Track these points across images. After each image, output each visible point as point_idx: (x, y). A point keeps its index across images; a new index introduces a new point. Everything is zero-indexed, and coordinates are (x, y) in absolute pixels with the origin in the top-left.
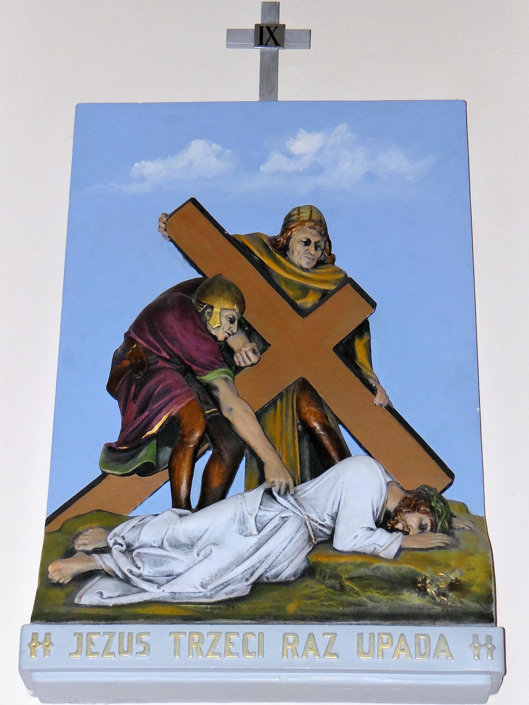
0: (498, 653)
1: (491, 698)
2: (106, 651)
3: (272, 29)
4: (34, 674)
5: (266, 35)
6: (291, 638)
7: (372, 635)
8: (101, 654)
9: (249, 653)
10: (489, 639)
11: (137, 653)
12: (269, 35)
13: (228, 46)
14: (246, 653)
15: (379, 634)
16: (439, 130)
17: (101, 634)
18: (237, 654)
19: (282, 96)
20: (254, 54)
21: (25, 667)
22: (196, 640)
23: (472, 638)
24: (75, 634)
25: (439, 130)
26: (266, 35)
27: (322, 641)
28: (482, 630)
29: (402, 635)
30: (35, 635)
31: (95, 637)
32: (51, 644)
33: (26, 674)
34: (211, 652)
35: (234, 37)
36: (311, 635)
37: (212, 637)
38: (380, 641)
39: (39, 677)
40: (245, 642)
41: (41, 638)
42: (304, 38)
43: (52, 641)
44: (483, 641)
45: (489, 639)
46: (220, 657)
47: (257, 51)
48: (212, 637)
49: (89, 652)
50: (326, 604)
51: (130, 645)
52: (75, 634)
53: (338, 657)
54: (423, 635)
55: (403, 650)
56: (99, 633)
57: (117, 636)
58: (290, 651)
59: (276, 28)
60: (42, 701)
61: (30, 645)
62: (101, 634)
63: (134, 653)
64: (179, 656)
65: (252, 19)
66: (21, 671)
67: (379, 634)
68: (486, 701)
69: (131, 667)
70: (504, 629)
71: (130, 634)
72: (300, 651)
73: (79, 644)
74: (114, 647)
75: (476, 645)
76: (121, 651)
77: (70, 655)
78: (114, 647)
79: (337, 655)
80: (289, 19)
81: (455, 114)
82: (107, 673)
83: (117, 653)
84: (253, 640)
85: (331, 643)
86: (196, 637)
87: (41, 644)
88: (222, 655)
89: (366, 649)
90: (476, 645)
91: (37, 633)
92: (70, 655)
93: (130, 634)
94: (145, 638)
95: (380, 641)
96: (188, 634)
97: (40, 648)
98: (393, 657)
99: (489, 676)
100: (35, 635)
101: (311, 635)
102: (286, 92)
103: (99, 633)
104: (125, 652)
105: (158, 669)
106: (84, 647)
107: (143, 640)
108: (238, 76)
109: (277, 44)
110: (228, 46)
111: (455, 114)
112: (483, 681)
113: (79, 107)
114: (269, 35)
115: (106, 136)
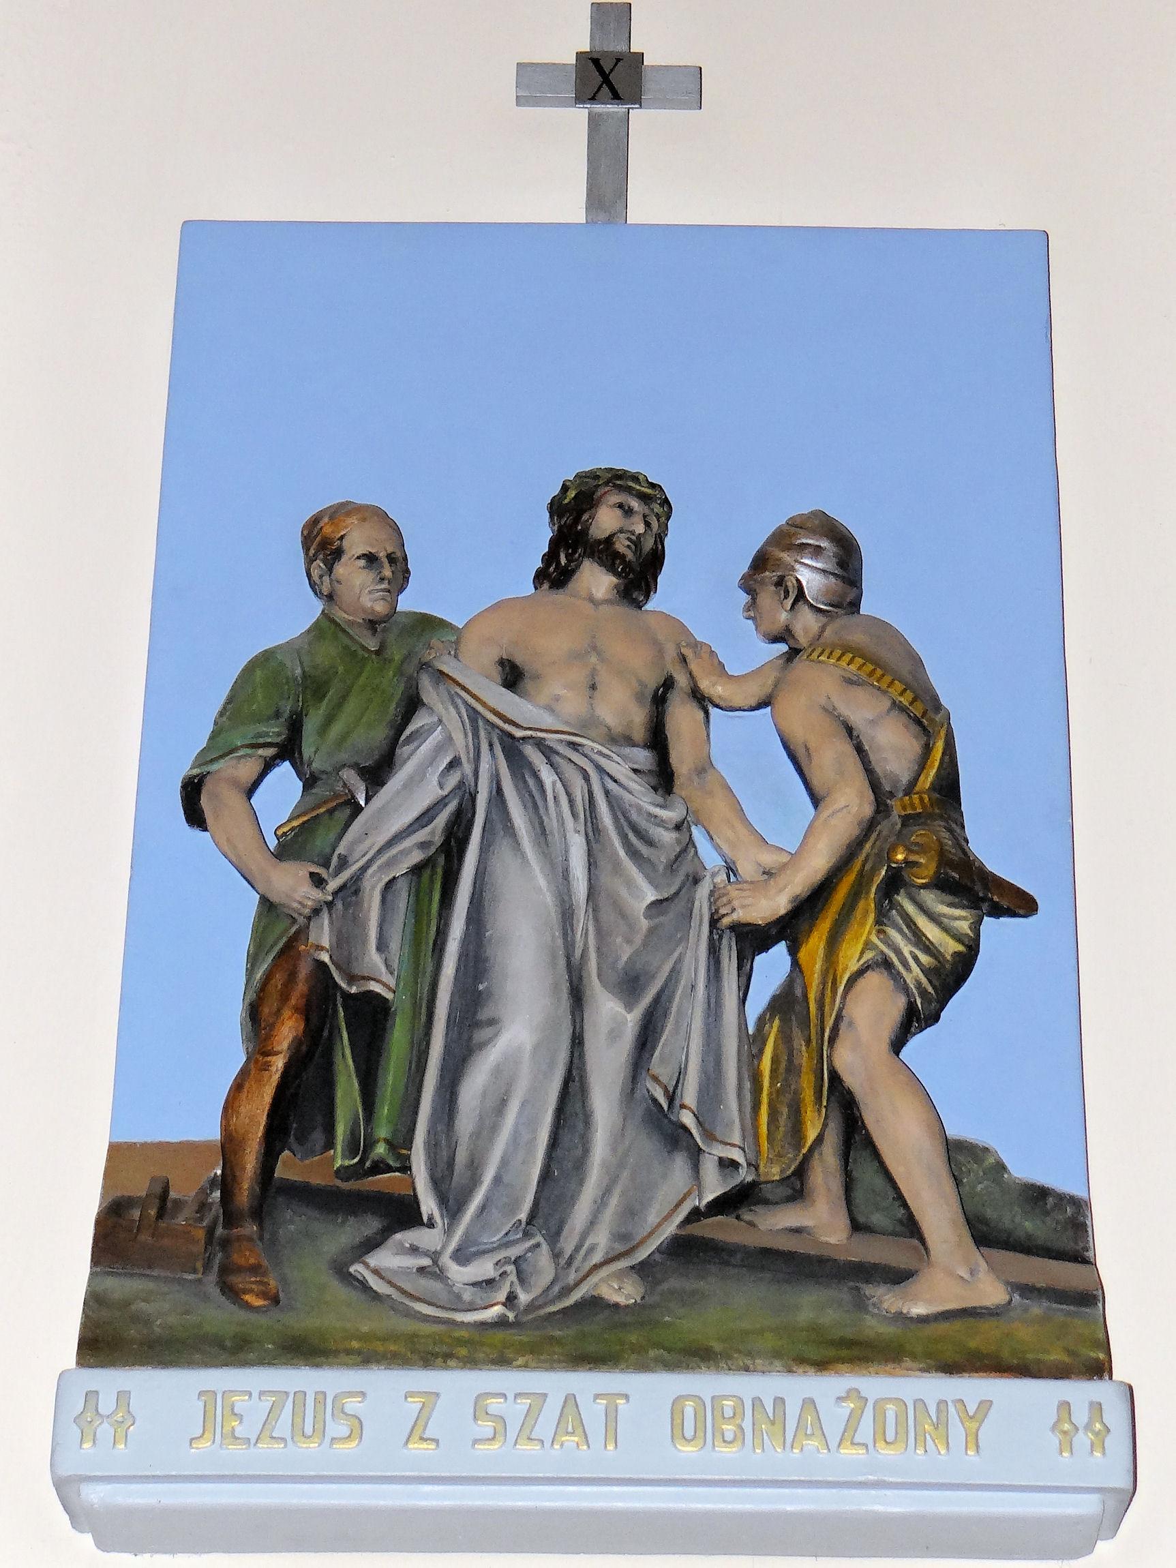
1: (1101, 1546)
2: (527, 1432)
3: (607, 66)
8: (253, 1441)
10: (1097, 1408)
12: (609, 77)
13: (520, 101)
14: (881, 1444)
16: (997, 289)
18: (283, 1440)
21: (65, 1471)
22: (728, 1413)
24: (597, 1396)
25: (997, 289)
27: (594, 1413)
28: (1079, 1392)
30: (91, 1396)
33: (65, 1487)
34: (416, 1437)
35: (533, 83)
36: (809, 1404)
38: (227, 1411)
39: (94, 1494)
41: (1081, 1415)
42: (689, 87)
44: (1081, 1415)
45: (1097, 1408)
46: (286, 1446)
47: (579, 116)
52: (201, 1394)
55: (573, 1433)
57: (291, 1396)
59: (618, 60)
60: (103, 1544)
65: (570, 39)
70: (1131, 1388)
73: (207, 1417)
74: (283, 1425)
75: (1067, 1427)
76: (298, 1431)
77: (473, 1445)
79: (437, 1441)
80: (653, 41)
81: (1014, 268)
84: (594, 1413)
88: (547, 1444)
90: (1067, 1427)
91: (97, 1392)
92: (473, 1445)
93: (321, 1396)
94: (352, 1405)
99: (1095, 1498)
100: (91, 1396)
101: (809, 1404)
102: (647, 203)
105: (372, 1477)
108: (537, 174)
109: (616, 97)
110: (520, 101)
111: (1014, 268)
112: (1088, 1505)
114: (609, 77)
115: (244, 289)
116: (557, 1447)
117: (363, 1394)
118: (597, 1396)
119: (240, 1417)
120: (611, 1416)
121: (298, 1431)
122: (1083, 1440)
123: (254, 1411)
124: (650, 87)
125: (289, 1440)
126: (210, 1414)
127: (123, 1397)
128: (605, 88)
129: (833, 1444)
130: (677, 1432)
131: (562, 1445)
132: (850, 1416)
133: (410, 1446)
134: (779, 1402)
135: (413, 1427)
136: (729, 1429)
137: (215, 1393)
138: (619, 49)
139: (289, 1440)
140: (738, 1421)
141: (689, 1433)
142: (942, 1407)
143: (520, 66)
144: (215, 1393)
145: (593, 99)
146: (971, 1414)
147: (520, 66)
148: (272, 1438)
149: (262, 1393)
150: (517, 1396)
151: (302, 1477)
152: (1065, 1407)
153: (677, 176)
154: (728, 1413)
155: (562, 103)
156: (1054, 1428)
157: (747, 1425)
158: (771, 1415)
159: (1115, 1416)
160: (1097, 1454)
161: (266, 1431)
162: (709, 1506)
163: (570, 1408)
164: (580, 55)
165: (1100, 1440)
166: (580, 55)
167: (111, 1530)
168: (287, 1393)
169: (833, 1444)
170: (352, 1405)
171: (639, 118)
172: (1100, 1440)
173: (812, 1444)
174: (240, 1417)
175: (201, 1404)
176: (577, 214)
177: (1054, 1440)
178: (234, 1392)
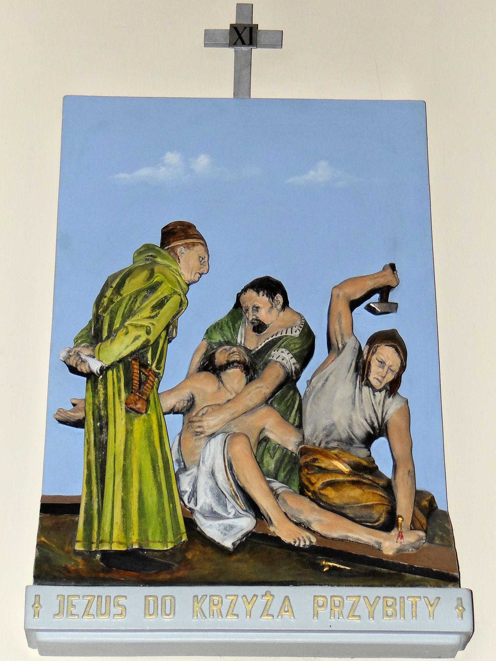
0: (467, 614)
2: (86, 613)
4: (39, 634)
5: (245, 36)
6: (321, 600)
8: (81, 615)
9: (387, 615)
11: (114, 615)
12: (244, 35)
13: (206, 45)
15: (331, 597)
17: (81, 597)
19: (255, 94)
23: (456, 602)
26: (245, 36)
28: (447, 593)
31: (75, 600)
33: (30, 633)
35: (211, 39)
38: (70, 604)
39: (43, 637)
40: (354, 606)
42: (276, 40)
47: (231, 51)
49: (108, 613)
50: (102, 575)
54: (392, 598)
55: (288, 611)
56: (420, 597)
59: (245, 28)
60: (41, 653)
61: (35, 606)
62: (81, 597)
63: (112, 615)
64: (404, 617)
65: (226, 19)
67: (331, 597)
74: (93, 610)
78: (93, 610)
79: (238, 616)
80: (263, 21)
83: (276, 615)
85: (354, 606)
94: (122, 601)
95: (70, 604)
98: (34, 616)
102: (258, 91)
104: (102, 615)
107: (120, 603)
108: (213, 76)
109: (243, 43)
110: (206, 45)
112: (454, 640)
113: (421, 107)
114: (244, 35)
115: (87, 122)
116: (279, 617)
117: (126, 597)
119: (74, 606)
123: (81, 604)
124: (261, 39)
125: (95, 616)
126: (62, 605)
129: (224, 614)
130: (146, 612)
132: (353, 605)
133: (228, 617)
135: (263, 611)
136: (390, 611)
137: (64, 596)
138: (245, 22)
139: (95, 616)
140: (341, 608)
141: (168, 612)
143: (258, 25)
144: (64, 596)
145: (235, 44)
147: (258, 25)
149: (83, 596)
150: (347, 597)
151: (265, 630)
153: (273, 77)
155: (224, 46)
156: (456, 608)
157: (398, 608)
161: (86, 613)
163: (287, 603)
164: (231, 25)
166: (231, 25)
167: (45, 649)
168: (360, 596)
170: (122, 601)
171: (256, 52)
173: (286, 615)
174: (74, 606)
175: (58, 601)
176: (232, 96)
178: (334, 596)
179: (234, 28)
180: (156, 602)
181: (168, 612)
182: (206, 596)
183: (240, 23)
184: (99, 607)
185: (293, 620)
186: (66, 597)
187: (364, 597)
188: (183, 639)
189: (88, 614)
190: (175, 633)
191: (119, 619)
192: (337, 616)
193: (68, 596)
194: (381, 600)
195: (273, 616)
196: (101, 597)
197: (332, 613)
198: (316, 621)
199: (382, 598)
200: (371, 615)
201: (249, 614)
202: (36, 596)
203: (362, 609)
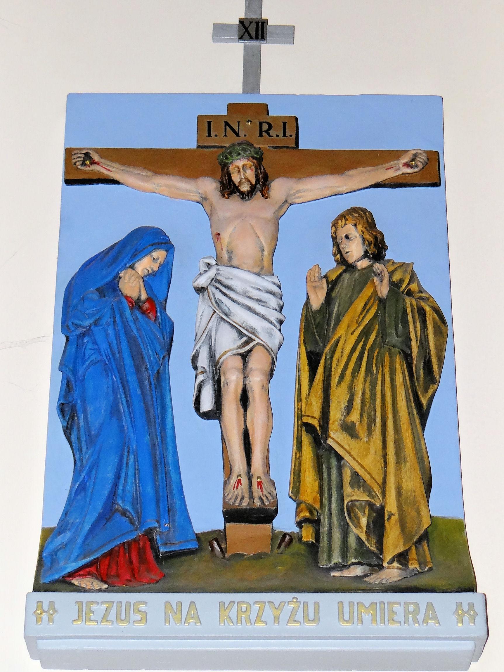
2: (105, 618)
3: (247, 25)
4: (40, 642)
6: (244, 606)
7: (351, 604)
10: (471, 606)
11: (134, 621)
12: (253, 30)
14: (342, 620)
17: (100, 604)
20: (237, 49)
28: (465, 597)
29: (191, 602)
30: (40, 603)
31: (94, 607)
32: (55, 611)
33: (31, 641)
35: (220, 31)
36: (192, 604)
37: (257, 606)
39: (43, 645)
40: (261, 610)
41: (46, 607)
42: (288, 34)
43: (56, 608)
45: (471, 606)
48: (257, 606)
49: (127, 619)
51: (128, 614)
53: (266, 624)
58: (243, 619)
59: (251, 22)
60: (44, 665)
61: (36, 614)
62: (100, 604)
64: (169, 624)
65: (235, 13)
66: (25, 637)
68: (467, 669)
69: (77, 635)
70: (485, 595)
71: (306, 604)
72: (420, 617)
73: (80, 611)
74: (112, 615)
76: (118, 618)
78: (112, 615)
80: (272, 15)
82: (97, 640)
86: (244, 606)
87: (45, 612)
89: (123, 617)
94: (142, 607)
96: (402, 604)
97: (45, 616)
98: (165, 624)
100: (40, 603)
101: (192, 604)
103: (97, 603)
106: (84, 613)
107: (140, 609)
109: (251, 38)
112: (469, 646)
114: (253, 30)
118: (256, 603)
119: (93, 612)
120: (317, 611)
121: (118, 618)
122: (466, 617)
123: (99, 609)
124: (269, 30)
127: (317, 604)
128: (246, 34)
129: (253, 622)
131: (189, 623)
134: (417, 605)
137: (82, 603)
140: (248, 613)
142: (179, 604)
144: (82, 603)
146: (277, 607)
148: (107, 621)
149: (102, 603)
150: (102, 603)
152: (459, 605)
154: (244, 609)
155: (232, 41)
158: (175, 610)
159: (479, 608)
160: (460, 625)
161: (105, 618)
162: (317, 648)
165: (473, 619)
167: (46, 659)
168: (113, 602)
169: (253, 622)
170: (142, 607)
172: (473, 619)
174: (93, 612)
176: (241, 92)
177: (455, 618)
179: (242, 22)
180: (382, 610)
181: (123, 618)
182: (234, 602)
183: (248, 17)
184: (119, 613)
185: (198, 626)
186: (356, 604)
187: (268, 602)
188: (202, 648)
189: (107, 621)
190: (122, 640)
191: (141, 626)
192: (183, 622)
193: (358, 603)
194: (236, 604)
195: (97, 622)
196: (121, 602)
197: (374, 619)
198: (240, 627)
199: (236, 603)
200: (277, 619)
201: (277, 619)
202: (314, 603)
203: (268, 613)
